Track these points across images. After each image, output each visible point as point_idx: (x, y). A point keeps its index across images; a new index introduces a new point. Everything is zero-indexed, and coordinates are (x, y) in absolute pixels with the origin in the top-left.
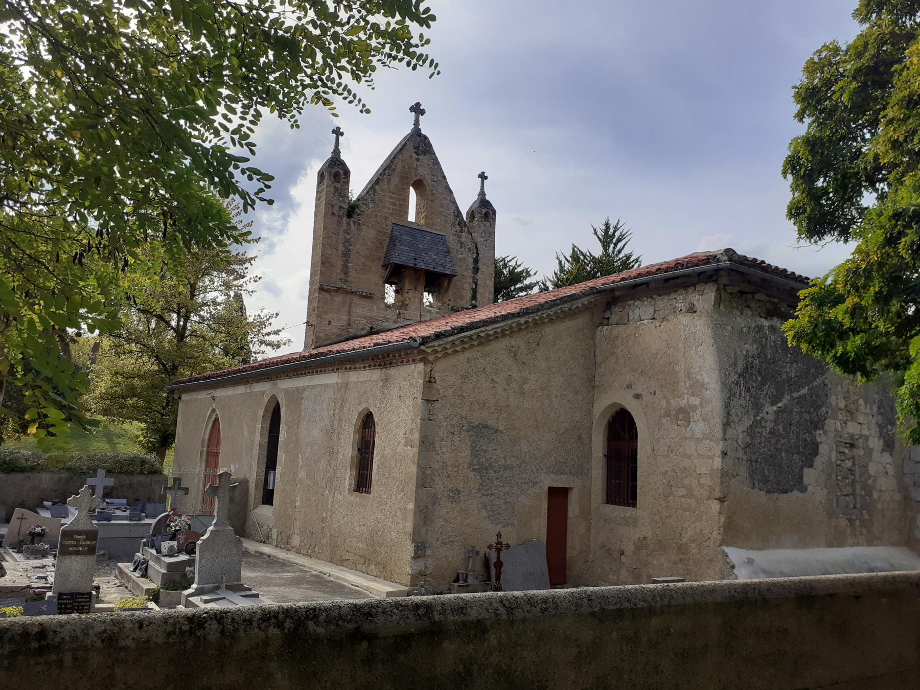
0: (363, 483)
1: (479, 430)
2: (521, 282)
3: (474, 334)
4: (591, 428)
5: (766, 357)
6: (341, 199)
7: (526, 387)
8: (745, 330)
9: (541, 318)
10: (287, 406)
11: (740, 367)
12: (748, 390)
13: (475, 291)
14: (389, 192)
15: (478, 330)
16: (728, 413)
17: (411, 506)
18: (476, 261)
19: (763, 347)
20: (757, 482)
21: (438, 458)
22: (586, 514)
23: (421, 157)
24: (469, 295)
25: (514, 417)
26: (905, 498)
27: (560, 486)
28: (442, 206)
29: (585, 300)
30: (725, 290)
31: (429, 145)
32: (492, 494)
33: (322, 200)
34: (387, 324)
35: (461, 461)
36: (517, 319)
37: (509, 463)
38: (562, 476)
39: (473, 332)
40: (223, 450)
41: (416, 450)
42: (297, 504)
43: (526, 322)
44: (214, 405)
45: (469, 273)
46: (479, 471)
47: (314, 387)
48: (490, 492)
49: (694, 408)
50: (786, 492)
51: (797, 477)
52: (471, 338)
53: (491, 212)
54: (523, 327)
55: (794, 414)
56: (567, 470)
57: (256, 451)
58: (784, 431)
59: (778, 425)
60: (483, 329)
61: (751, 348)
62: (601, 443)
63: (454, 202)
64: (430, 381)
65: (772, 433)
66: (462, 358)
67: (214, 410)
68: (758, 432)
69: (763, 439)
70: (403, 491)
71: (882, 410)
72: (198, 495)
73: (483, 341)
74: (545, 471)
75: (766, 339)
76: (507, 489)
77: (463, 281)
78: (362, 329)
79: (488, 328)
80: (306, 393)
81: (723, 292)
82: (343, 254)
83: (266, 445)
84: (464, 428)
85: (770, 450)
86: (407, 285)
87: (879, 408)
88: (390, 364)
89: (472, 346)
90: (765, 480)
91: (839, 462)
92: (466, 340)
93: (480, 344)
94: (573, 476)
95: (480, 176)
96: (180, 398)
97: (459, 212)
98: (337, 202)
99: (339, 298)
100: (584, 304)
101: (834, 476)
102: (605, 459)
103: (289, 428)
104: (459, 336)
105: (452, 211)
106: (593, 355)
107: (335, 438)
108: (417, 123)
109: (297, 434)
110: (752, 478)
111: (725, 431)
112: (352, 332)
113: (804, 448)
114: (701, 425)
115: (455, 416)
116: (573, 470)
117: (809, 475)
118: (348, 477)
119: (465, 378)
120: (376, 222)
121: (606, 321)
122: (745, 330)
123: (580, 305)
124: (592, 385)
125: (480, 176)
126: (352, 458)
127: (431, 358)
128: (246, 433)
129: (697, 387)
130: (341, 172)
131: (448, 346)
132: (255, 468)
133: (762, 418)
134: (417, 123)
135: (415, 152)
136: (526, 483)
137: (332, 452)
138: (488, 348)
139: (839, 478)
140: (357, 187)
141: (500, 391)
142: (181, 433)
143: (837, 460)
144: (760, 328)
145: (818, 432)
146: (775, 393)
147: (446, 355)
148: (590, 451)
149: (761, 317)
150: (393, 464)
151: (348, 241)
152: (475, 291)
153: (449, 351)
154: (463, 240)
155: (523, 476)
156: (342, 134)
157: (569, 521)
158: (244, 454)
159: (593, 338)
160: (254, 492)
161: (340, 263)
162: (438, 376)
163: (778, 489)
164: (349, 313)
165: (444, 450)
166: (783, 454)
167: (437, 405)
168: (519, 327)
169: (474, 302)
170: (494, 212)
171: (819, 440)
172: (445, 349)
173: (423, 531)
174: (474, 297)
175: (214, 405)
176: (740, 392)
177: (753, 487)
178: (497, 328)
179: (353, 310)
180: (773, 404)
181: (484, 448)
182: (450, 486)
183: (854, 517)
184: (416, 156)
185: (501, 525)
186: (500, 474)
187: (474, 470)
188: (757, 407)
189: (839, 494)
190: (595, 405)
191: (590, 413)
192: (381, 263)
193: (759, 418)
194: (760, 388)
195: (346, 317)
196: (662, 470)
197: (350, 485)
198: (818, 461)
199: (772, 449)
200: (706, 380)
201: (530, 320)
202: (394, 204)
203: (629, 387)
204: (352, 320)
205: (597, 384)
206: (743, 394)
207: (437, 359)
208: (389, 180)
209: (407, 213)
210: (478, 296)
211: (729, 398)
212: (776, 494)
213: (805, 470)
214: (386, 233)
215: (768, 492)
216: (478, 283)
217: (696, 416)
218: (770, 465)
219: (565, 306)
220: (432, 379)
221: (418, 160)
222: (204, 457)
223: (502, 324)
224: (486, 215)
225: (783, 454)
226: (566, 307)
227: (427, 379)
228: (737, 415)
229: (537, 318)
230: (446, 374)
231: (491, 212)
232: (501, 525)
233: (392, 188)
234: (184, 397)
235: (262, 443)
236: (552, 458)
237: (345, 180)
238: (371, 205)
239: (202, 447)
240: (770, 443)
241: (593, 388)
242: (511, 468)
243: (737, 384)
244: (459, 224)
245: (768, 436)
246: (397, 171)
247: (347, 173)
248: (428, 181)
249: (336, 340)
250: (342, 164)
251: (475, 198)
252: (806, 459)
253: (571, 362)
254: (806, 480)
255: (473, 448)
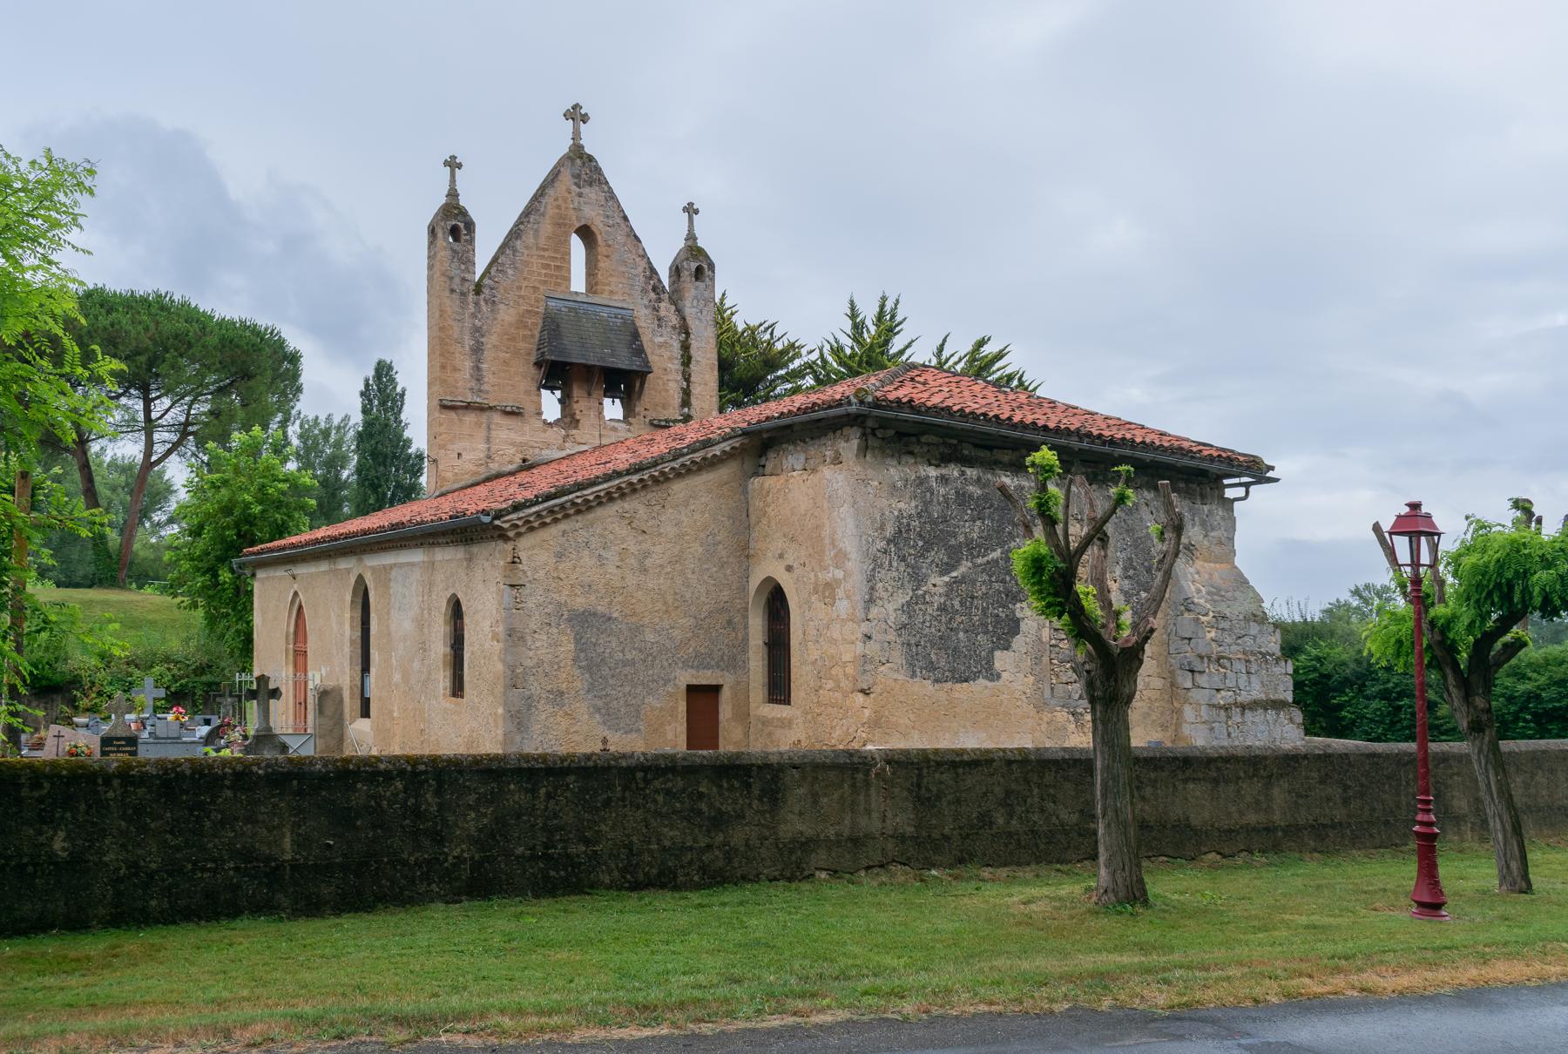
0: (457, 689)
1: (583, 621)
2: (785, 365)
3: (567, 502)
4: (746, 609)
5: (930, 515)
6: (463, 267)
7: (648, 562)
8: (899, 484)
9: (662, 473)
10: (376, 588)
11: (890, 531)
12: (903, 559)
13: (687, 393)
14: (538, 248)
15: (571, 497)
16: (872, 588)
17: (500, 711)
18: (685, 347)
19: (926, 504)
20: (918, 670)
21: (531, 654)
22: (743, 715)
23: (586, 190)
24: (677, 399)
25: (634, 601)
26: (1172, 685)
27: (704, 683)
28: (625, 263)
29: (726, 446)
30: (874, 435)
31: (598, 170)
32: (607, 695)
33: (435, 269)
34: (548, 452)
35: (562, 656)
36: (626, 478)
37: (629, 656)
38: (706, 671)
39: (566, 498)
40: (312, 646)
41: (501, 645)
42: (395, 715)
43: (641, 480)
44: (296, 587)
45: (676, 366)
46: (589, 669)
47: (401, 566)
48: (604, 693)
49: (838, 582)
50: (966, 681)
51: (983, 663)
52: (562, 506)
53: (706, 266)
54: (639, 486)
55: (978, 584)
56: (713, 663)
57: (347, 649)
58: (961, 606)
59: (951, 599)
60: (578, 494)
61: (908, 506)
62: (760, 628)
63: (644, 256)
64: (514, 562)
65: (942, 608)
66: (555, 530)
67: (296, 594)
68: (920, 610)
69: (928, 618)
70: (493, 694)
71: (1131, 572)
72: (287, 709)
73: (585, 507)
74: (680, 665)
75: (932, 494)
76: (627, 689)
77: (666, 378)
78: (510, 462)
79: (585, 492)
80: (394, 573)
81: (870, 438)
82: (471, 349)
83: (359, 641)
84: (564, 617)
85: (939, 631)
86: (577, 392)
87: (1125, 569)
88: (472, 539)
89: (567, 516)
90: (931, 667)
91: (1053, 642)
92: (556, 509)
93: (579, 512)
94: (723, 670)
95: (685, 209)
96: (254, 575)
97: (653, 271)
98: (458, 272)
99: (470, 418)
100: (724, 451)
101: (1046, 659)
102: (766, 649)
103: (379, 619)
104: (546, 505)
105: (640, 269)
106: (744, 515)
107: (426, 630)
108: (576, 135)
109: (388, 626)
110: (912, 665)
111: (867, 609)
112: (494, 467)
113: (994, 627)
114: (845, 602)
115: (550, 603)
116: (722, 664)
117: (1001, 660)
118: (443, 680)
119: (560, 556)
120: (520, 297)
121: (759, 470)
122: (899, 484)
123: (718, 453)
124: (745, 553)
125: (685, 209)
126: (445, 656)
127: (511, 534)
128: (334, 625)
129: (841, 557)
130: (462, 225)
131: (532, 519)
132: (347, 670)
133: (925, 592)
134: (576, 135)
135: (576, 184)
136: (653, 681)
137: (423, 648)
138: (591, 516)
139: (1055, 662)
140: (485, 248)
141: (611, 569)
142: (260, 624)
143: (1051, 639)
144: (922, 481)
145: (1018, 605)
146: (946, 560)
147: (532, 529)
148: (746, 639)
149: (930, 464)
150: (482, 662)
151: (477, 330)
152: (687, 393)
153: (536, 524)
154: (663, 313)
155: (651, 672)
156: (459, 166)
157: (721, 726)
158: (335, 652)
159: (745, 492)
160: (350, 704)
161: (468, 364)
162: (523, 555)
163: (953, 677)
164: (488, 440)
165: (538, 644)
166: (961, 635)
167: (525, 591)
168: (633, 489)
169: (686, 410)
170: (711, 266)
171: (1018, 614)
172: (529, 522)
173: (518, 738)
174: (686, 402)
175: (296, 587)
176: (890, 561)
177: (913, 675)
178: (600, 491)
179: (494, 433)
180: (942, 574)
181: (593, 640)
182: (549, 687)
183: (1079, 710)
184: (578, 190)
185: (622, 731)
186: (618, 671)
187: (580, 667)
188: (918, 579)
189: (1054, 681)
190: (750, 579)
191: (743, 589)
192: (533, 359)
193: (920, 592)
194: (922, 555)
195: (483, 446)
196: (812, 658)
197: (445, 689)
198: (1018, 642)
199: (943, 629)
200: (849, 548)
201: (645, 477)
202: (547, 266)
203: (781, 556)
204: (492, 450)
205: (752, 552)
206: (895, 564)
207: (519, 535)
208: (537, 231)
209: (568, 279)
210: (693, 401)
211: (874, 569)
212: (950, 683)
213: (997, 654)
214: (537, 313)
215: (937, 681)
216: (692, 379)
217: (840, 593)
218: (940, 649)
219: (697, 455)
220: (516, 559)
221: (580, 195)
222: (291, 657)
223: (605, 486)
224: (699, 271)
225: (961, 635)
226: (698, 456)
227: (509, 560)
228: (887, 590)
229: (656, 474)
230: (534, 552)
231: (706, 266)
232: (622, 731)
233: (542, 242)
234: (260, 574)
235: (354, 638)
236: (691, 649)
237: (468, 237)
238: (510, 272)
239: (287, 643)
240: (940, 621)
241: (747, 557)
242: (633, 663)
243: (885, 553)
244: (654, 289)
245: (935, 614)
246: (547, 216)
247: (470, 226)
248: (598, 226)
249: (470, 482)
250: (463, 213)
251: (681, 244)
252: (998, 639)
253: (713, 526)
254: (998, 665)
255: (577, 641)
